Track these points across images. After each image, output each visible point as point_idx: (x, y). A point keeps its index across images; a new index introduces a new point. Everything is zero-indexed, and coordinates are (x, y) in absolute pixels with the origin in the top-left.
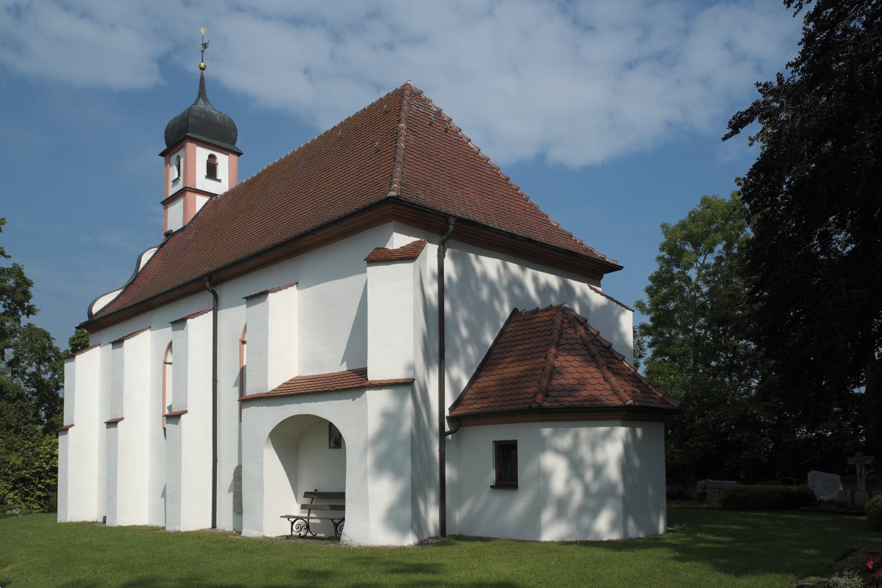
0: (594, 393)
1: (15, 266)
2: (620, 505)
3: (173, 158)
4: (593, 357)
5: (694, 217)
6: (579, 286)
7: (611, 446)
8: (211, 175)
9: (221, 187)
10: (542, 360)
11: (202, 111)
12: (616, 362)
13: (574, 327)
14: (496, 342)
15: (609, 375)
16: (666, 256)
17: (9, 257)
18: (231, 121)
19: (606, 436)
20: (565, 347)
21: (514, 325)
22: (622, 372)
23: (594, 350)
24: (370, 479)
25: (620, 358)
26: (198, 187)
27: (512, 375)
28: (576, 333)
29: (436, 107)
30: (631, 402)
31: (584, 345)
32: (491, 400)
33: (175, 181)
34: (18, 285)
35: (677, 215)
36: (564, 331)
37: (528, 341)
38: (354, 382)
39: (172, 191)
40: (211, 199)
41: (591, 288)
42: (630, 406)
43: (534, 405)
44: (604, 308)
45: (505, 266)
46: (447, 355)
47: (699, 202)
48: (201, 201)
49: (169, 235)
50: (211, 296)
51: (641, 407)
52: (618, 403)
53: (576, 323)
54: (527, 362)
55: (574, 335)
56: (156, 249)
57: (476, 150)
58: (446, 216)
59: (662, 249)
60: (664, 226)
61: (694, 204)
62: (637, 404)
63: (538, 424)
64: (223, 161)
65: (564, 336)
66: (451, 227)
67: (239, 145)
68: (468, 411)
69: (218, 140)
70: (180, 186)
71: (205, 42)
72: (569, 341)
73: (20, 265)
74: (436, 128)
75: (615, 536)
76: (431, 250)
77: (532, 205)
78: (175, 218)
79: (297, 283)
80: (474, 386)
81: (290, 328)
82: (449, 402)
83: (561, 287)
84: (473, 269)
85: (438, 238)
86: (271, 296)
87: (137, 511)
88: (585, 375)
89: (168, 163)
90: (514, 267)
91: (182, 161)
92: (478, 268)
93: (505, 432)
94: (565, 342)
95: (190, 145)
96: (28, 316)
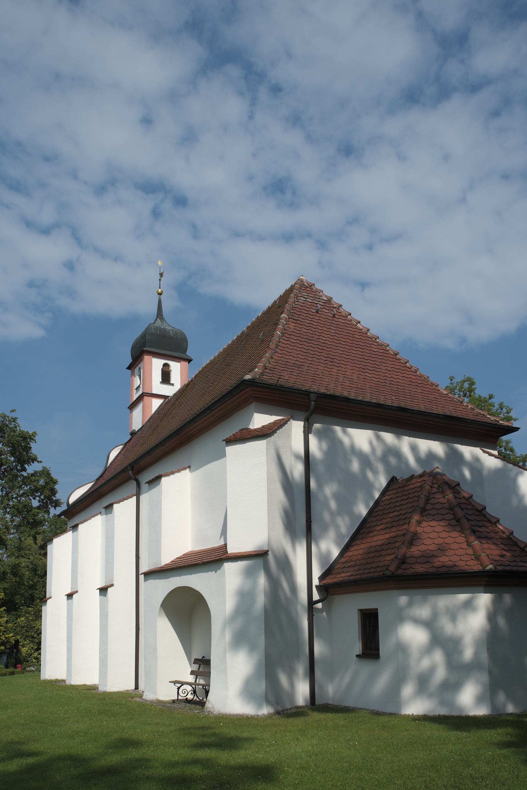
0: (455, 559)
1: (44, 468)
2: (485, 677)
3: (137, 370)
4: (458, 521)
6: (468, 451)
7: (473, 616)
8: (163, 380)
9: (169, 391)
10: (406, 526)
11: (157, 328)
12: (488, 524)
13: (443, 492)
14: (371, 512)
15: (472, 538)
17: (41, 462)
18: (182, 334)
19: (468, 605)
20: (430, 512)
21: (391, 492)
22: (492, 535)
23: (460, 513)
24: (229, 655)
25: (494, 521)
26: (154, 392)
27: (379, 543)
28: (444, 497)
29: (326, 296)
30: (491, 566)
31: (451, 509)
32: (356, 568)
33: (138, 388)
34: (47, 483)
36: (431, 496)
37: (397, 509)
38: (214, 559)
39: (135, 397)
41: (484, 452)
42: (490, 571)
43: (387, 573)
44: (497, 472)
45: (378, 438)
46: (315, 527)
48: (156, 403)
49: (133, 434)
50: (134, 484)
51: (503, 572)
52: (477, 568)
53: (446, 487)
54: (394, 529)
55: (442, 500)
56: (121, 447)
58: (307, 393)
62: (500, 568)
63: (395, 592)
64: (176, 367)
65: (431, 501)
66: (313, 403)
67: (189, 353)
68: (341, 579)
69: (170, 351)
70: (140, 393)
71: (161, 272)
72: (435, 506)
73: (48, 468)
74: (332, 315)
75: (482, 711)
76: (297, 427)
77: (421, 376)
78: (137, 420)
79: (189, 467)
80: (349, 554)
81: (180, 508)
82: (316, 573)
83: (446, 454)
84: (341, 443)
85: (304, 415)
86: (164, 479)
87: (86, 675)
88: (446, 541)
89: (133, 374)
90: (388, 437)
91: (142, 371)
92: (346, 441)
93: (367, 601)
94: (431, 507)
95: (146, 358)
96: (55, 508)
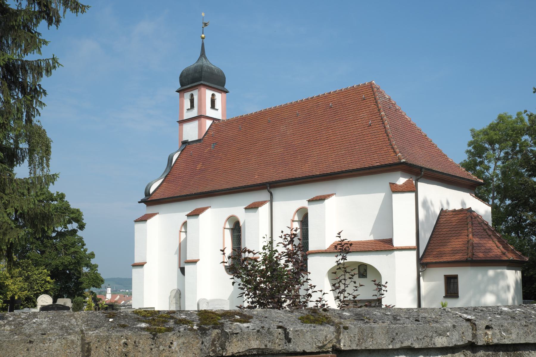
4: (490, 236)
5: (492, 127)
16: (473, 150)
18: (222, 72)
35: (482, 124)
40: (213, 122)
42: (512, 260)
47: (496, 117)
49: (185, 143)
57: (409, 119)
59: (469, 145)
60: (472, 131)
61: (493, 119)
64: (219, 96)
67: (226, 87)
77: (439, 150)
78: (191, 132)
89: (182, 97)
93: (451, 271)
